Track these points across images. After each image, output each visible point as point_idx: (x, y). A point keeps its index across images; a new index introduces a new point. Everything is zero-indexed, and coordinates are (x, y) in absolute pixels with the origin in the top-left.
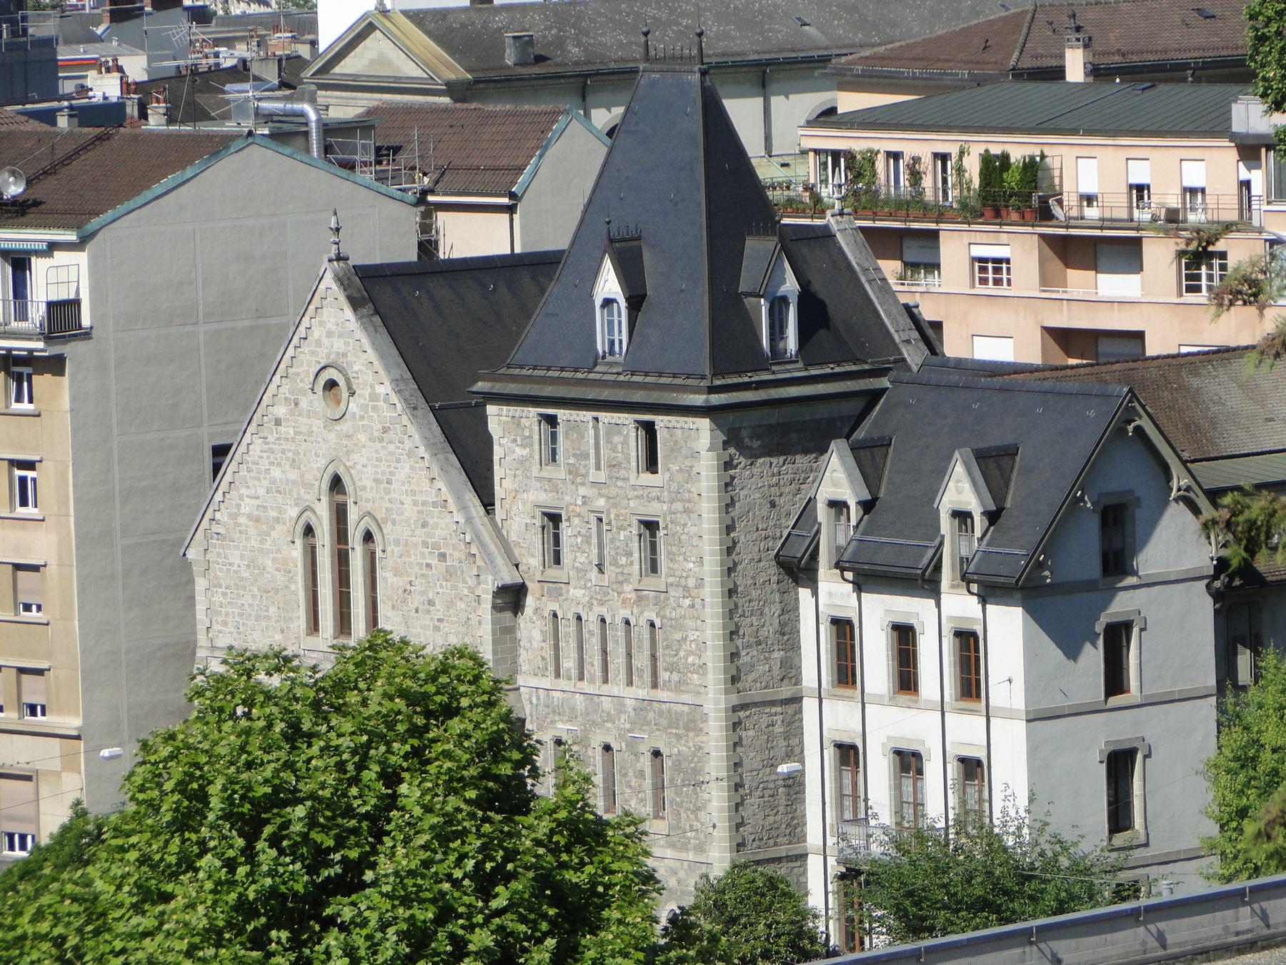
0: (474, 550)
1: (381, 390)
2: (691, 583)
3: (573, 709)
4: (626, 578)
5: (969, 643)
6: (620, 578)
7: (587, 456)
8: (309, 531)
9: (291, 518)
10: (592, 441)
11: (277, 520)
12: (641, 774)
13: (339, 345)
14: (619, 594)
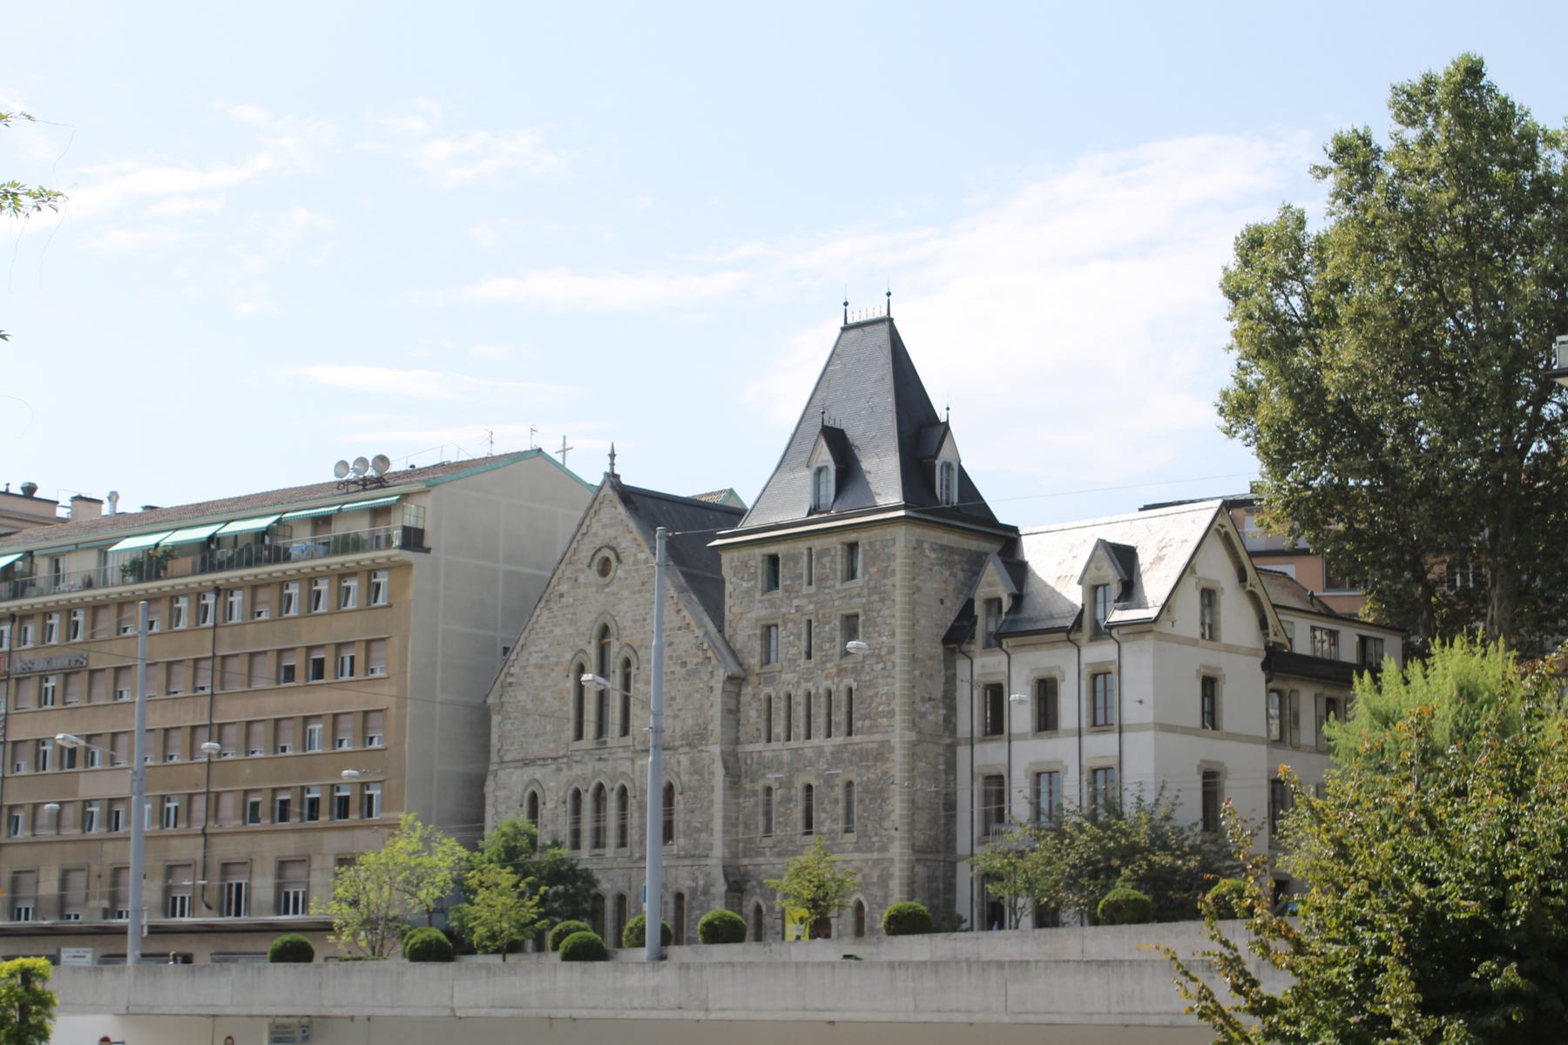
0: (710, 654)
1: (642, 556)
3: (780, 763)
4: (829, 658)
7: (801, 576)
10: (805, 565)
11: (557, 664)
12: (836, 801)
13: (611, 532)
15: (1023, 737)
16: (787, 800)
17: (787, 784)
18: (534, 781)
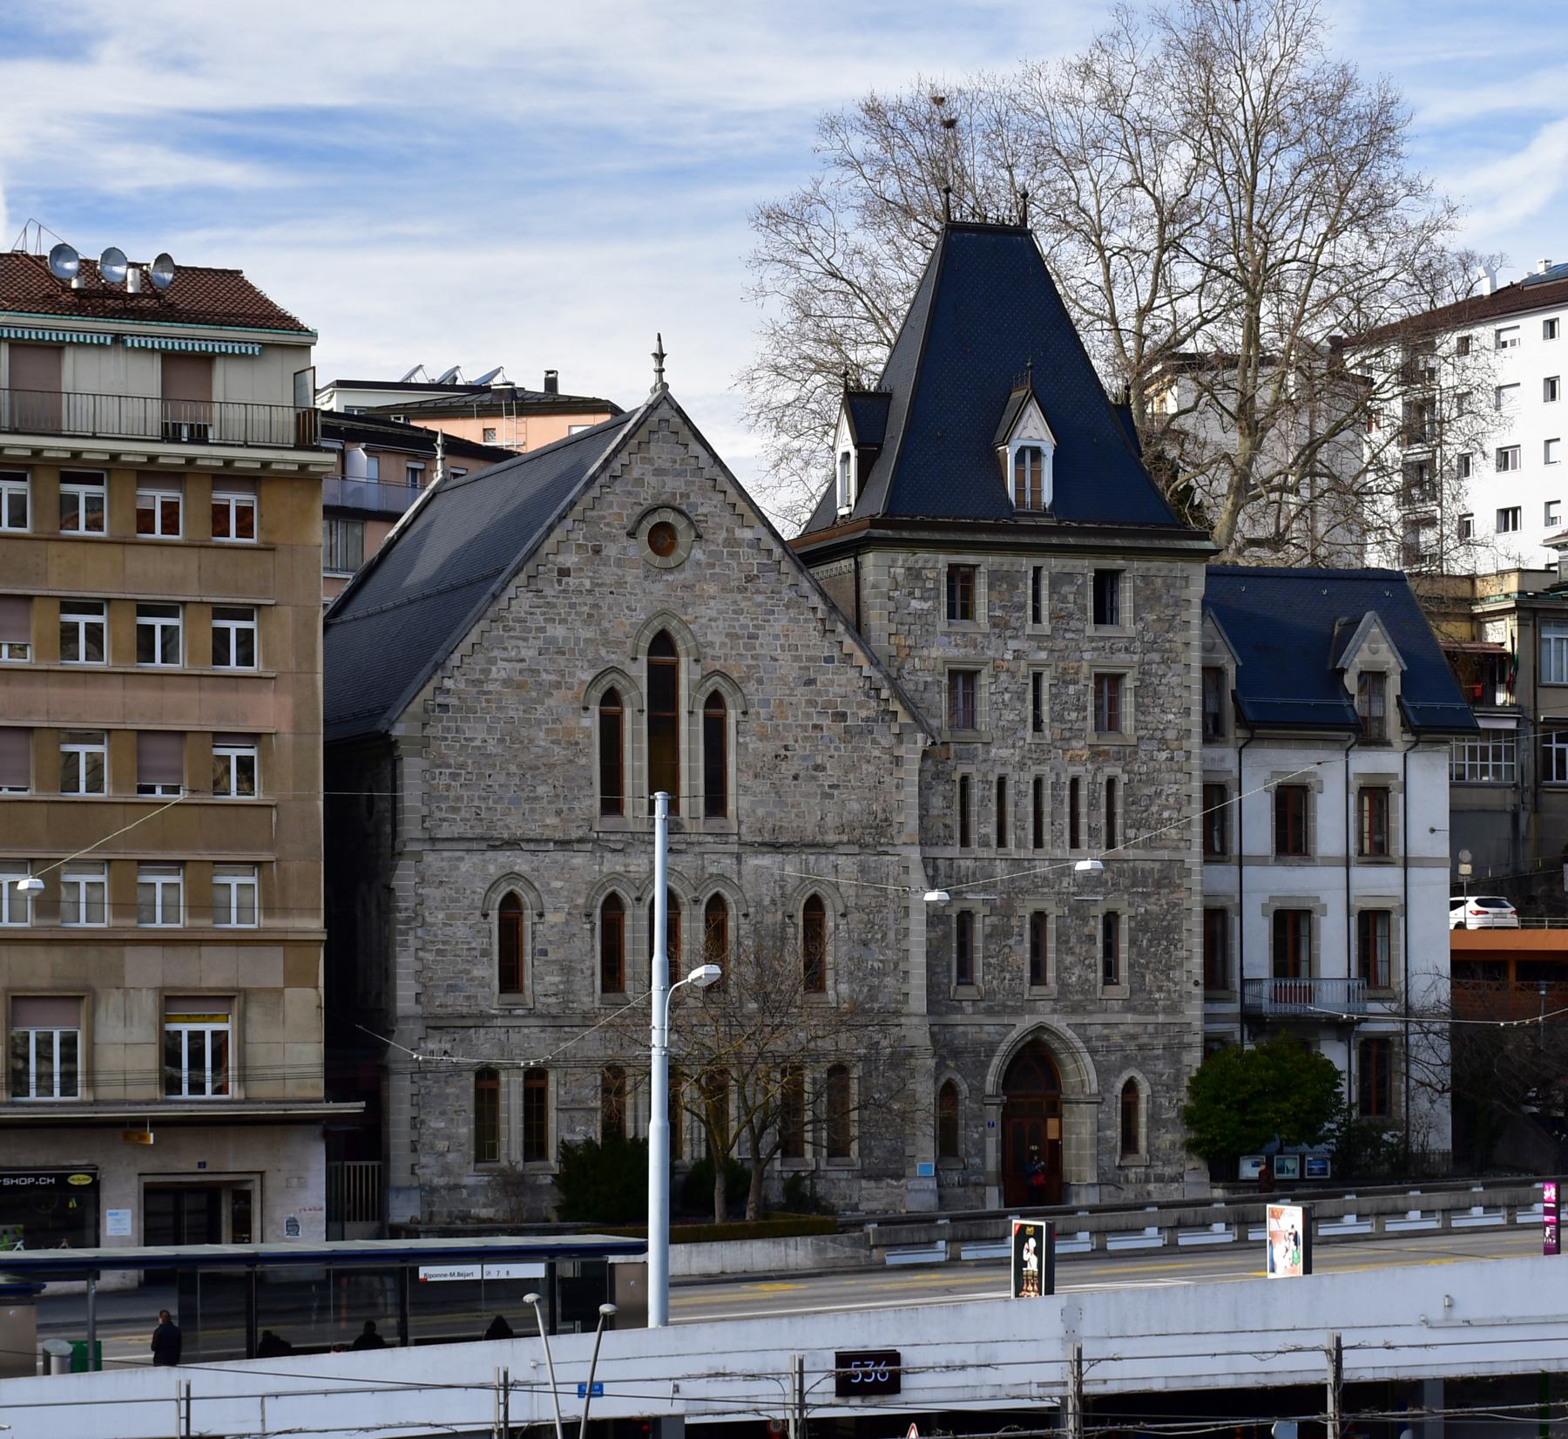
2: (1171, 734)
5: (1376, 798)
6: (1067, 734)
7: (1022, 607)
8: (611, 698)
9: (582, 682)
11: (558, 685)
12: (1091, 938)
14: (1065, 751)
15: (1260, 861)
16: (999, 933)
17: (1004, 911)
18: (513, 876)
